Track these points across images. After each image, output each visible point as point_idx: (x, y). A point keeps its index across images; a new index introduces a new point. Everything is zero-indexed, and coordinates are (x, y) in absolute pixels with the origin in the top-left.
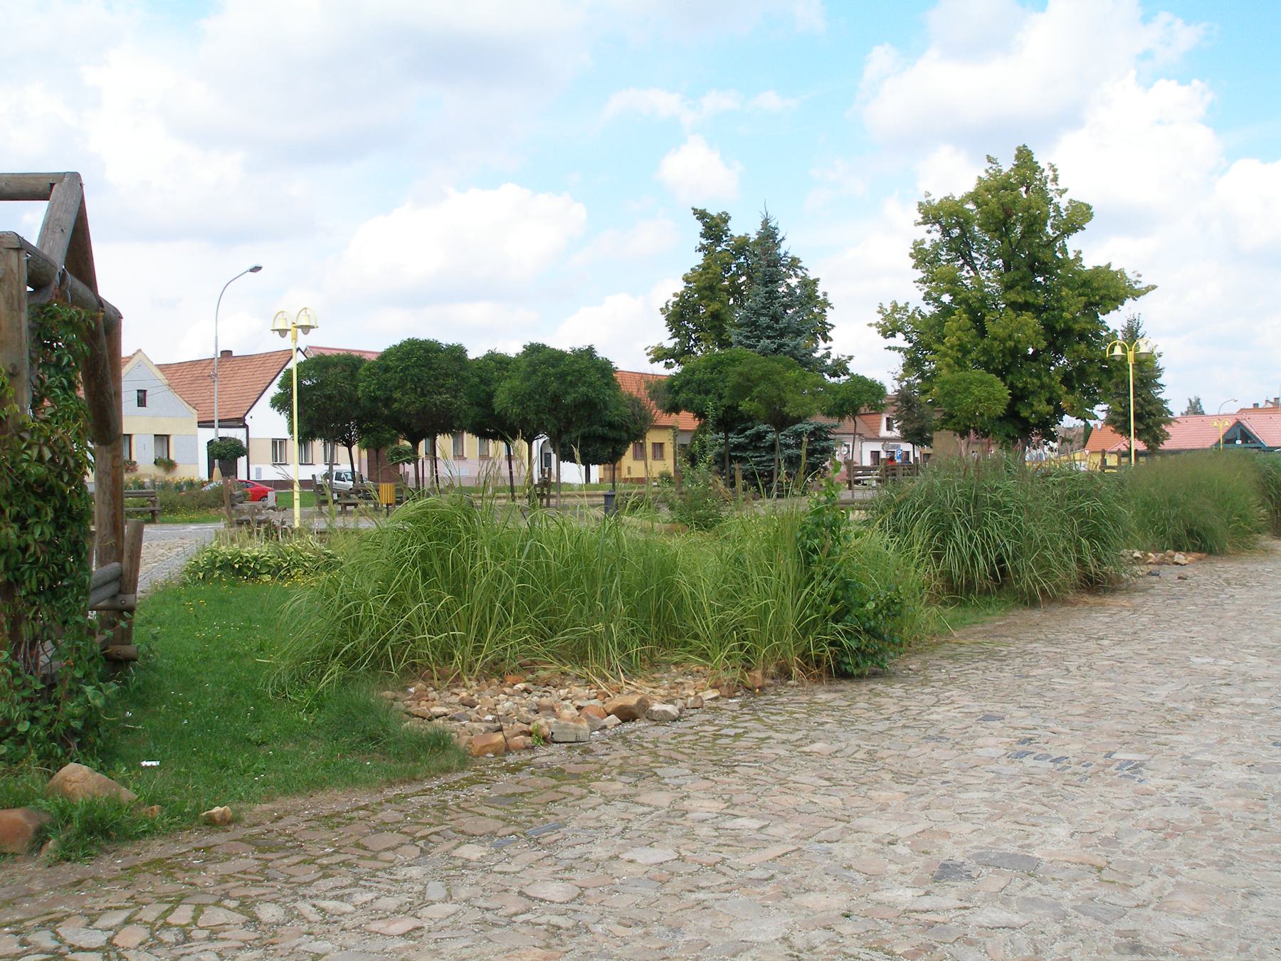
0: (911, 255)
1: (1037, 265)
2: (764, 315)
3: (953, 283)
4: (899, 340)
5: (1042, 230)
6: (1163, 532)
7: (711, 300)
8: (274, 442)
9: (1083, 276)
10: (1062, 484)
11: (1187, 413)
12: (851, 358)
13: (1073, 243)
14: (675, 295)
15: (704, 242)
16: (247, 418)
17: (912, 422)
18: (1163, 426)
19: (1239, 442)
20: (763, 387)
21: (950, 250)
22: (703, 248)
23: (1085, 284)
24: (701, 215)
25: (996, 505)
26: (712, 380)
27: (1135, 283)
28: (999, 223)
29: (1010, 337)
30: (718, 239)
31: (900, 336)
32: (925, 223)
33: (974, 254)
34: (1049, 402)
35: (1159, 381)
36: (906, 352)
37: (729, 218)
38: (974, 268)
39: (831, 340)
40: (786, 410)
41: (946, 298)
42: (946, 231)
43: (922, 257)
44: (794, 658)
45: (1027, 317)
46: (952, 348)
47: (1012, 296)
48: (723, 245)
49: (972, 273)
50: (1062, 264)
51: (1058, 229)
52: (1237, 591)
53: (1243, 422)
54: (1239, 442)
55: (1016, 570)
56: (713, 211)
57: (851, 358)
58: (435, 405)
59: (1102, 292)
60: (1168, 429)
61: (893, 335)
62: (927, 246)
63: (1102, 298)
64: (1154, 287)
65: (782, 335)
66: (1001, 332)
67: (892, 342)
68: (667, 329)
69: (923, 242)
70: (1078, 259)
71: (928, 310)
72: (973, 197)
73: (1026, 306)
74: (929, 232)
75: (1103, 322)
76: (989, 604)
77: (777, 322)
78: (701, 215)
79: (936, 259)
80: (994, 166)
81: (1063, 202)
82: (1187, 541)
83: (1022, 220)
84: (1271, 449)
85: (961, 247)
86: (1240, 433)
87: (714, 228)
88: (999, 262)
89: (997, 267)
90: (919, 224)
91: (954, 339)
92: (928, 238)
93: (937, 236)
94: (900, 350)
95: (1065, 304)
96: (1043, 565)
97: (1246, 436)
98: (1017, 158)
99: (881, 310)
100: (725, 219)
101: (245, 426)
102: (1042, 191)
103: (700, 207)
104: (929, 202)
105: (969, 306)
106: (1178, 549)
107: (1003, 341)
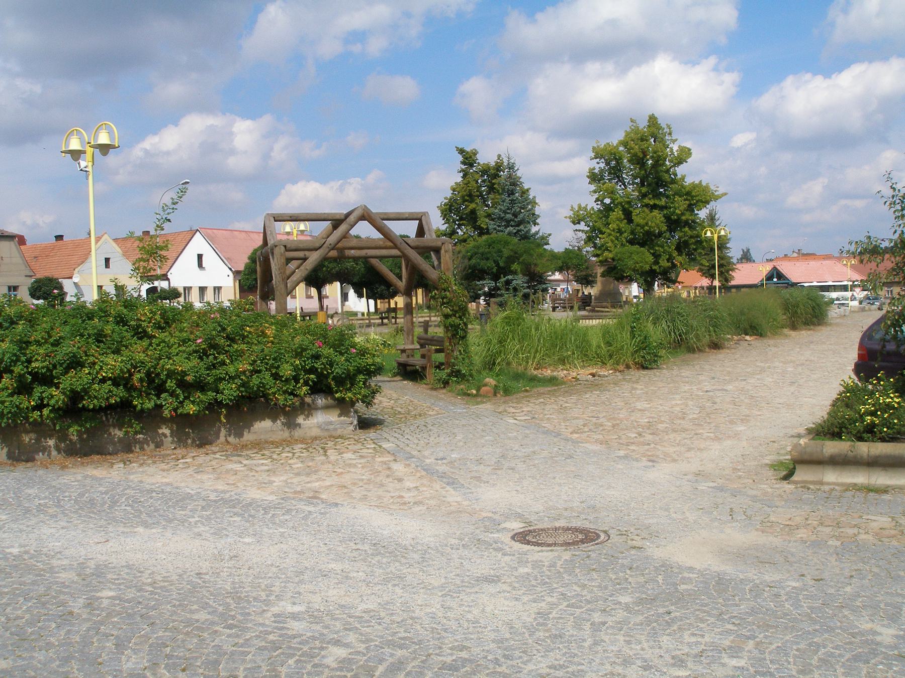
0: (588, 176)
1: (660, 182)
2: (508, 213)
3: (612, 193)
4: (582, 226)
5: (664, 164)
6: (739, 327)
7: (471, 202)
8: (215, 288)
9: (687, 189)
10: (701, 305)
11: (741, 259)
12: (550, 235)
13: (680, 170)
14: (446, 198)
15: (463, 167)
16: (169, 274)
17: (581, 271)
18: (731, 272)
19: (775, 280)
20: (525, 256)
21: (610, 173)
22: (462, 171)
23: (688, 193)
24: (461, 151)
25: (679, 313)
26: (490, 252)
27: (716, 191)
28: (639, 161)
29: (647, 224)
30: (471, 165)
31: (582, 223)
32: (596, 158)
33: (624, 176)
34: (668, 260)
35: (728, 245)
36: (586, 232)
37: (478, 153)
38: (625, 185)
39: (538, 224)
40: (538, 269)
41: (607, 201)
42: (608, 163)
43: (594, 177)
44: (631, 363)
45: (656, 212)
46: (614, 230)
47: (646, 201)
48: (474, 169)
49: (623, 186)
50: (673, 182)
51: (672, 162)
52: (773, 349)
53: (778, 267)
54: (775, 280)
55: (686, 339)
56: (468, 149)
57: (550, 235)
58: (347, 269)
59: (697, 198)
60: (733, 274)
61: (579, 223)
62: (596, 171)
63: (697, 201)
64: (726, 194)
65: (518, 225)
66: (642, 222)
67: (578, 227)
68: (442, 218)
69: (594, 169)
70: (683, 178)
71: (597, 207)
72: (625, 144)
73: (654, 207)
74: (598, 163)
75: (697, 214)
76: (677, 352)
77: (516, 217)
78: (461, 151)
79: (602, 178)
80: (635, 124)
81: (675, 148)
82: (750, 331)
83: (652, 157)
84: (794, 285)
85: (616, 172)
86: (776, 275)
87: (469, 159)
88: (638, 180)
89: (637, 184)
90: (593, 159)
91: (615, 226)
92: (597, 166)
93: (602, 165)
94: (583, 231)
95: (677, 205)
96: (697, 336)
97: (780, 276)
98: (649, 121)
99: (572, 209)
100: (475, 153)
101: (168, 279)
102: (663, 141)
103: (460, 147)
104: (598, 146)
105: (623, 206)
106: (746, 334)
107: (642, 227)
